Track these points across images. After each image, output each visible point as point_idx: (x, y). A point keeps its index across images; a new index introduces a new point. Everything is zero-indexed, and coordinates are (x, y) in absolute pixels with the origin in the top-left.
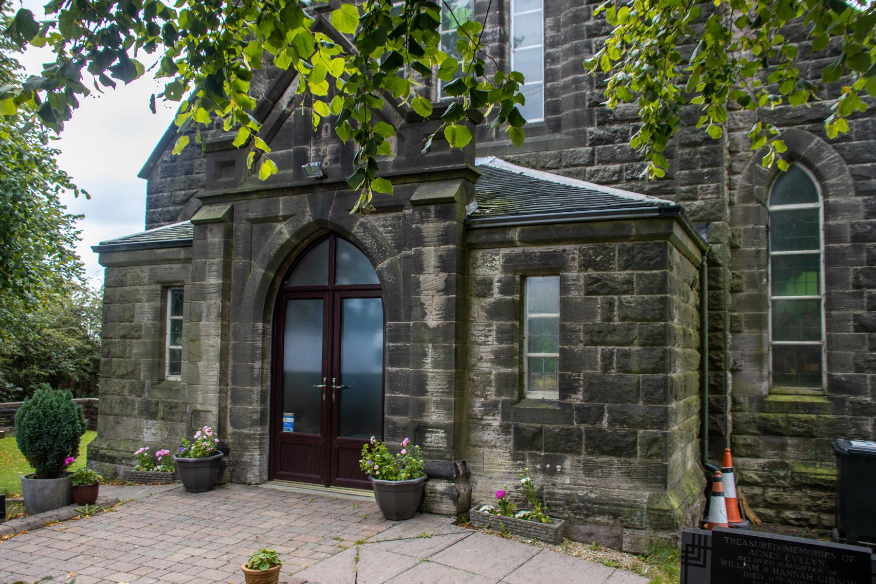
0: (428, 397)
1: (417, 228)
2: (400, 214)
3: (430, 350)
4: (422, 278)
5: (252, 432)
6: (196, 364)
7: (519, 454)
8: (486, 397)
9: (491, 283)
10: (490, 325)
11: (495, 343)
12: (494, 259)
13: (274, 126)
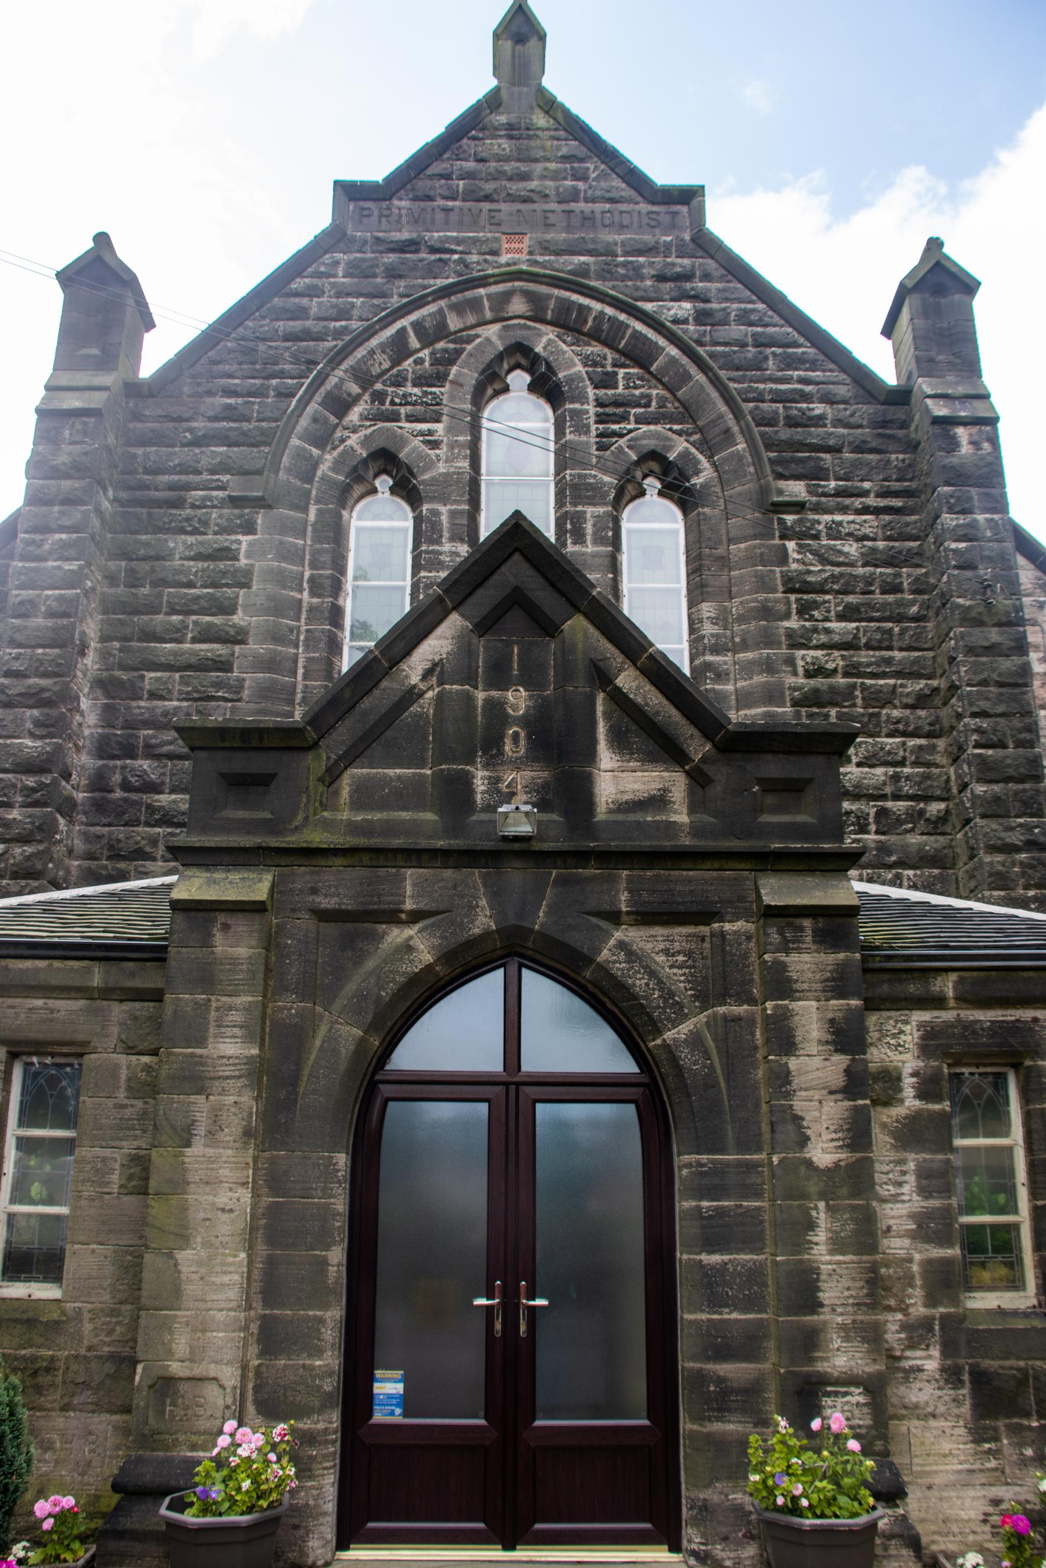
0: (825, 1316)
1: (776, 962)
2: (704, 930)
3: (821, 1214)
4: (793, 1063)
5: (321, 1426)
6: (170, 1256)
7: (986, 1428)
8: (904, 1311)
9: (899, 1079)
10: (901, 1162)
11: (915, 1197)
12: (901, 1032)
13: (385, 715)
